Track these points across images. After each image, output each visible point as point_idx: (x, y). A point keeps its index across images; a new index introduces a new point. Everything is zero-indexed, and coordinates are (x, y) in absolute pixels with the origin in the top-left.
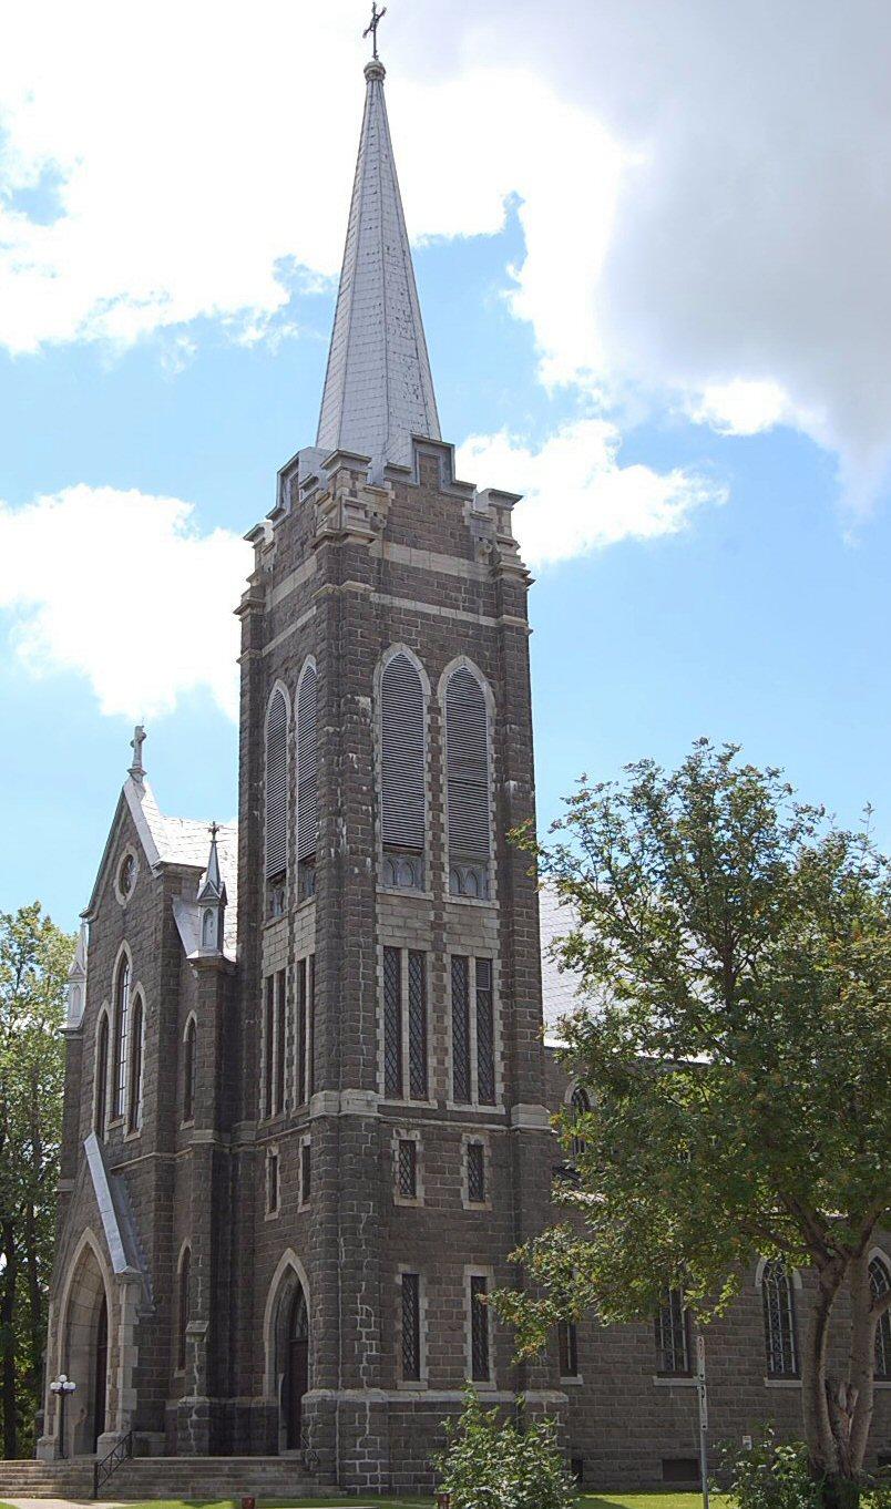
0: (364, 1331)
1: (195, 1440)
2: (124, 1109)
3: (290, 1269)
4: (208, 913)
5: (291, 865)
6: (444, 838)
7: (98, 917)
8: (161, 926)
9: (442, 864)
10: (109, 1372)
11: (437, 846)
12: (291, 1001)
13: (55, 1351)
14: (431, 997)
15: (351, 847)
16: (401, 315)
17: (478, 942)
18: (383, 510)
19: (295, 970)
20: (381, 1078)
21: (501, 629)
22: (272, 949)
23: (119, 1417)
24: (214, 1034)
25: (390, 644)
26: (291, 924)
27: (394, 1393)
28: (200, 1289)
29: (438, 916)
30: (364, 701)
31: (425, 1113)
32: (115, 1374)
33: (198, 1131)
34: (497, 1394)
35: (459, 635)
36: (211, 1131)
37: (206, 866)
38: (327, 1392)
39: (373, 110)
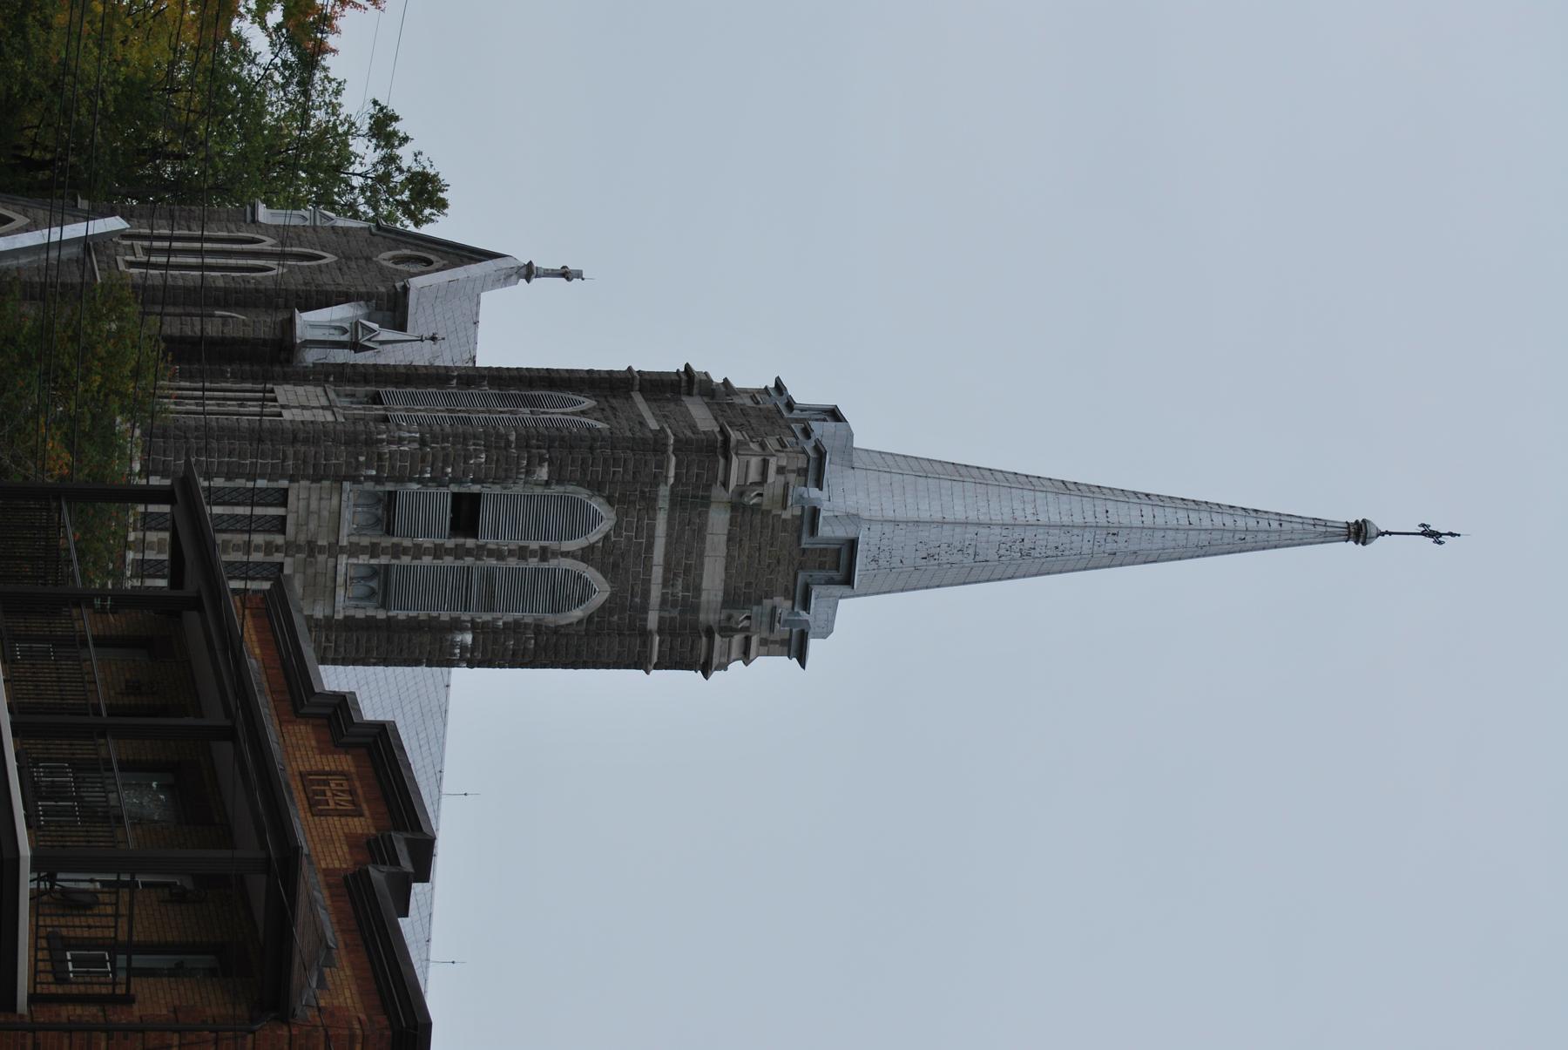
5: (385, 409)
8: (340, 289)
9: (377, 556)
11: (397, 551)
12: (241, 406)
15: (385, 453)
16: (1028, 544)
18: (766, 503)
19: (275, 409)
21: (645, 634)
25: (613, 506)
26: (323, 408)
29: (321, 550)
30: (543, 473)
35: (632, 587)
39: (1306, 526)
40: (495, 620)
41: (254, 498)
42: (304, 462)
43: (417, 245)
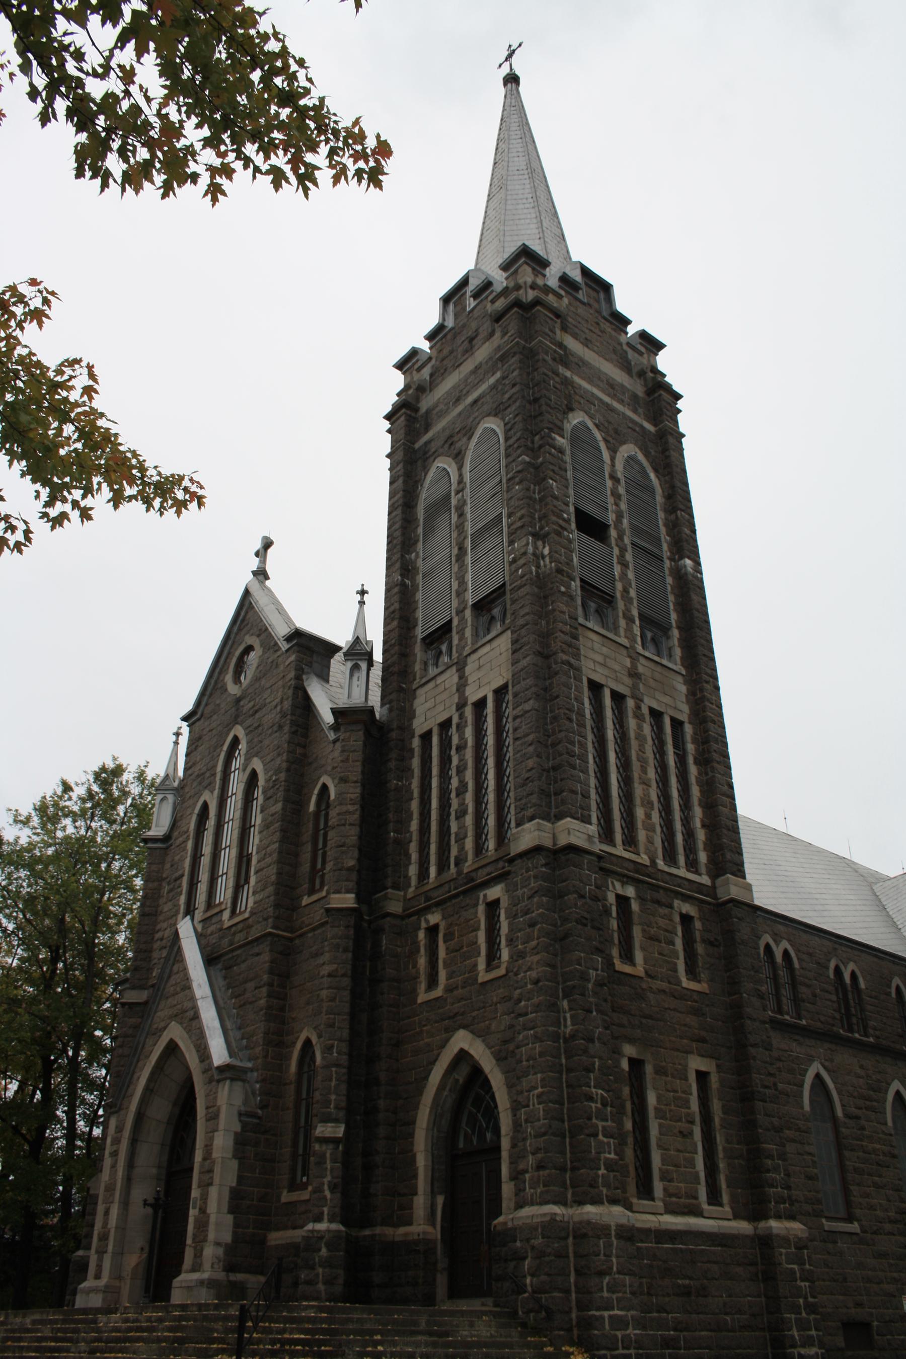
0: (600, 1124)
1: (325, 1283)
2: (224, 893)
6: (633, 593)
7: (202, 715)
10: (195, 1193)
17: (667, 700)
22: (430, 704)
23: (209, 1252)
24: (358, 790)
28: (333, 1084)
29: (633, 666)
32: (204, 1198)
33: (337, 896)
34: (734, 1224)
36: (353, 896)
43: (220, 673)
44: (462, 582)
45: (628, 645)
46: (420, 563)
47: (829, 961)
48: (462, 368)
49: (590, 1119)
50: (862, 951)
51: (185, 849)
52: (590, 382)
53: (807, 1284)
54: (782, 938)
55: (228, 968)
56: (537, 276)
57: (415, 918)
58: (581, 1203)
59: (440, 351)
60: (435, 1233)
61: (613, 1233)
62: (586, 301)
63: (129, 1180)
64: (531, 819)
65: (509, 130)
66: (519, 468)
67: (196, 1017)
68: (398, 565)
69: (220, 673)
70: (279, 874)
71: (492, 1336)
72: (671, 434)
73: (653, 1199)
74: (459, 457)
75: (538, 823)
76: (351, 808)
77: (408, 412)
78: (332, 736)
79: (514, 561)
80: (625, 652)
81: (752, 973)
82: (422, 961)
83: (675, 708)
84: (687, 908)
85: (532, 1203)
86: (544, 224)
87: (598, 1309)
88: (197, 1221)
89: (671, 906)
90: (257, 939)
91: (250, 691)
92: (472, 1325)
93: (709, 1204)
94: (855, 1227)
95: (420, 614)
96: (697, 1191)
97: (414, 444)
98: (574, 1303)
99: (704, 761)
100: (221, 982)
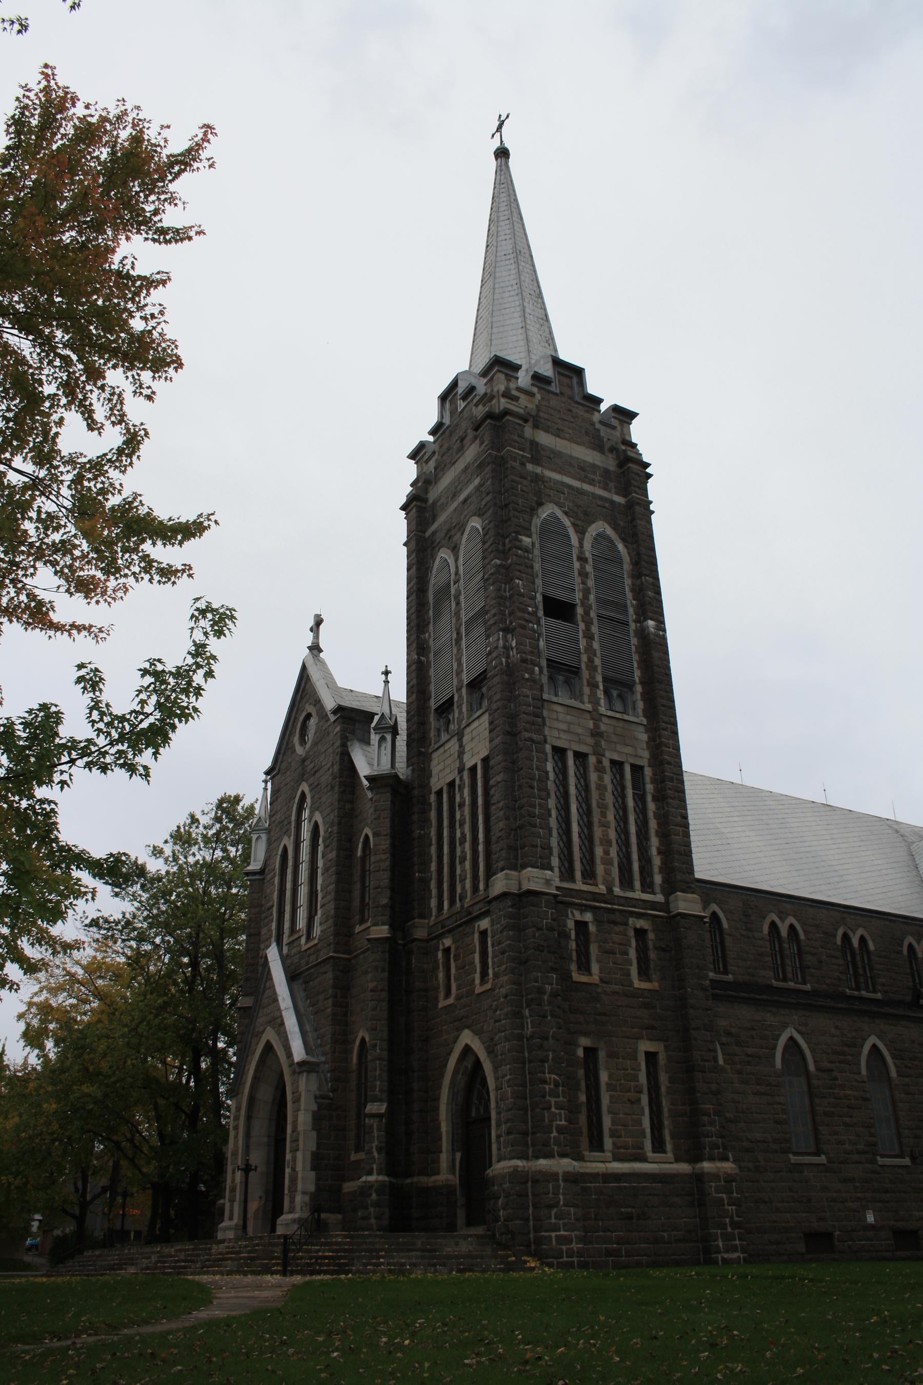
0: (553, 1100)
2: (301, 923)
3: (467, 1049)
4: (382, 739)
5: (459, 689)
6: (597, 661)
7: (279, 771)
10: (288, 1156)
13: (236, 1142)
14: (595, 795)
17: (628, 750)
20: (555, 862)
22: (440, 767)
23: (299, 1198)
24: (388, 842)
26: (460, 740)
27: (582, 1164)
28: (378, 1073)
29: (597, 726)
30: (526, 540)
31: (596, 897)
32: (294, 1159)
34: (675, 1166)
36: (386, 927)
37: (381, 695)
38: (519, 1163)
40: (632, 605)
41: (562, 772)
42: (533, 724)
43: (290, 735)
44: (460, 664)
45: (591, 710)
46: (431, 642)
47: (837, 930)
48: (457, 465)
49: (544, 1096)
50: (871, 917)
51: (273, 884)
52: (561, 471)
53: (734, 1208)
54: (789, 915)
55: (306, 982)
56: (510, 380)
57: (435, 941)
58: (537, 1158)
59: (441, 447)
60: (455, 1180)
61: (561, 1178)
62: (558, 391)
63: (247, 1147)
64: (502, 870)
65: (498, 211)
66: (492, 571)
67: (282, 1024)
68: (415, 645)
69: (290, 735)
70: (337, 908)
71: (470, 1251)
72: (639, 504)
73: (603, 1151)
74: (455, 549)
75: (506, 874)
76: (383, 857)
77: (419, 504)
78: (369, 795)
79: (490, 653)
80: (588, 716)
81: (697, 971)
82: (441, 975)
83: (636, 756)
84: (641, 923)
85: (505, 1159)
86: (528, 310)
87: (546, 1231)
88: (290, 1176)
89: (626, 924)
90: (323, 961)
91: (311, 753)
92: (457, 1244)
93: (654, 1152)
94: (823, 1159)
95: (432, 688)
96: (643, 1144)
97: (424, 532)
98: (531, 1228)
99: (660, 798)
100: (301, 995)
